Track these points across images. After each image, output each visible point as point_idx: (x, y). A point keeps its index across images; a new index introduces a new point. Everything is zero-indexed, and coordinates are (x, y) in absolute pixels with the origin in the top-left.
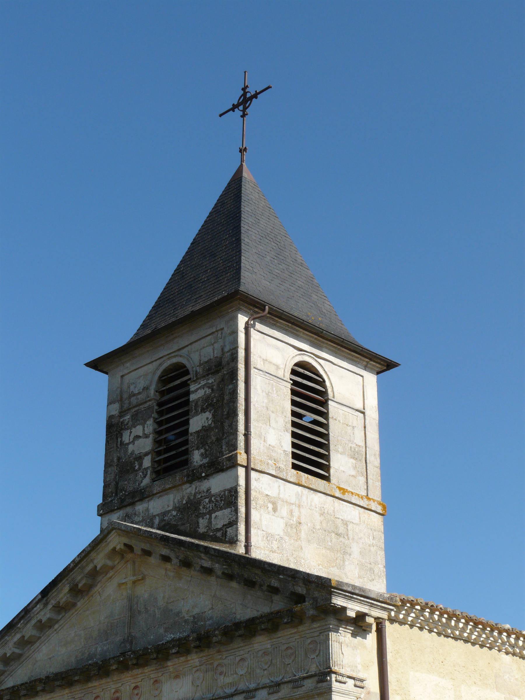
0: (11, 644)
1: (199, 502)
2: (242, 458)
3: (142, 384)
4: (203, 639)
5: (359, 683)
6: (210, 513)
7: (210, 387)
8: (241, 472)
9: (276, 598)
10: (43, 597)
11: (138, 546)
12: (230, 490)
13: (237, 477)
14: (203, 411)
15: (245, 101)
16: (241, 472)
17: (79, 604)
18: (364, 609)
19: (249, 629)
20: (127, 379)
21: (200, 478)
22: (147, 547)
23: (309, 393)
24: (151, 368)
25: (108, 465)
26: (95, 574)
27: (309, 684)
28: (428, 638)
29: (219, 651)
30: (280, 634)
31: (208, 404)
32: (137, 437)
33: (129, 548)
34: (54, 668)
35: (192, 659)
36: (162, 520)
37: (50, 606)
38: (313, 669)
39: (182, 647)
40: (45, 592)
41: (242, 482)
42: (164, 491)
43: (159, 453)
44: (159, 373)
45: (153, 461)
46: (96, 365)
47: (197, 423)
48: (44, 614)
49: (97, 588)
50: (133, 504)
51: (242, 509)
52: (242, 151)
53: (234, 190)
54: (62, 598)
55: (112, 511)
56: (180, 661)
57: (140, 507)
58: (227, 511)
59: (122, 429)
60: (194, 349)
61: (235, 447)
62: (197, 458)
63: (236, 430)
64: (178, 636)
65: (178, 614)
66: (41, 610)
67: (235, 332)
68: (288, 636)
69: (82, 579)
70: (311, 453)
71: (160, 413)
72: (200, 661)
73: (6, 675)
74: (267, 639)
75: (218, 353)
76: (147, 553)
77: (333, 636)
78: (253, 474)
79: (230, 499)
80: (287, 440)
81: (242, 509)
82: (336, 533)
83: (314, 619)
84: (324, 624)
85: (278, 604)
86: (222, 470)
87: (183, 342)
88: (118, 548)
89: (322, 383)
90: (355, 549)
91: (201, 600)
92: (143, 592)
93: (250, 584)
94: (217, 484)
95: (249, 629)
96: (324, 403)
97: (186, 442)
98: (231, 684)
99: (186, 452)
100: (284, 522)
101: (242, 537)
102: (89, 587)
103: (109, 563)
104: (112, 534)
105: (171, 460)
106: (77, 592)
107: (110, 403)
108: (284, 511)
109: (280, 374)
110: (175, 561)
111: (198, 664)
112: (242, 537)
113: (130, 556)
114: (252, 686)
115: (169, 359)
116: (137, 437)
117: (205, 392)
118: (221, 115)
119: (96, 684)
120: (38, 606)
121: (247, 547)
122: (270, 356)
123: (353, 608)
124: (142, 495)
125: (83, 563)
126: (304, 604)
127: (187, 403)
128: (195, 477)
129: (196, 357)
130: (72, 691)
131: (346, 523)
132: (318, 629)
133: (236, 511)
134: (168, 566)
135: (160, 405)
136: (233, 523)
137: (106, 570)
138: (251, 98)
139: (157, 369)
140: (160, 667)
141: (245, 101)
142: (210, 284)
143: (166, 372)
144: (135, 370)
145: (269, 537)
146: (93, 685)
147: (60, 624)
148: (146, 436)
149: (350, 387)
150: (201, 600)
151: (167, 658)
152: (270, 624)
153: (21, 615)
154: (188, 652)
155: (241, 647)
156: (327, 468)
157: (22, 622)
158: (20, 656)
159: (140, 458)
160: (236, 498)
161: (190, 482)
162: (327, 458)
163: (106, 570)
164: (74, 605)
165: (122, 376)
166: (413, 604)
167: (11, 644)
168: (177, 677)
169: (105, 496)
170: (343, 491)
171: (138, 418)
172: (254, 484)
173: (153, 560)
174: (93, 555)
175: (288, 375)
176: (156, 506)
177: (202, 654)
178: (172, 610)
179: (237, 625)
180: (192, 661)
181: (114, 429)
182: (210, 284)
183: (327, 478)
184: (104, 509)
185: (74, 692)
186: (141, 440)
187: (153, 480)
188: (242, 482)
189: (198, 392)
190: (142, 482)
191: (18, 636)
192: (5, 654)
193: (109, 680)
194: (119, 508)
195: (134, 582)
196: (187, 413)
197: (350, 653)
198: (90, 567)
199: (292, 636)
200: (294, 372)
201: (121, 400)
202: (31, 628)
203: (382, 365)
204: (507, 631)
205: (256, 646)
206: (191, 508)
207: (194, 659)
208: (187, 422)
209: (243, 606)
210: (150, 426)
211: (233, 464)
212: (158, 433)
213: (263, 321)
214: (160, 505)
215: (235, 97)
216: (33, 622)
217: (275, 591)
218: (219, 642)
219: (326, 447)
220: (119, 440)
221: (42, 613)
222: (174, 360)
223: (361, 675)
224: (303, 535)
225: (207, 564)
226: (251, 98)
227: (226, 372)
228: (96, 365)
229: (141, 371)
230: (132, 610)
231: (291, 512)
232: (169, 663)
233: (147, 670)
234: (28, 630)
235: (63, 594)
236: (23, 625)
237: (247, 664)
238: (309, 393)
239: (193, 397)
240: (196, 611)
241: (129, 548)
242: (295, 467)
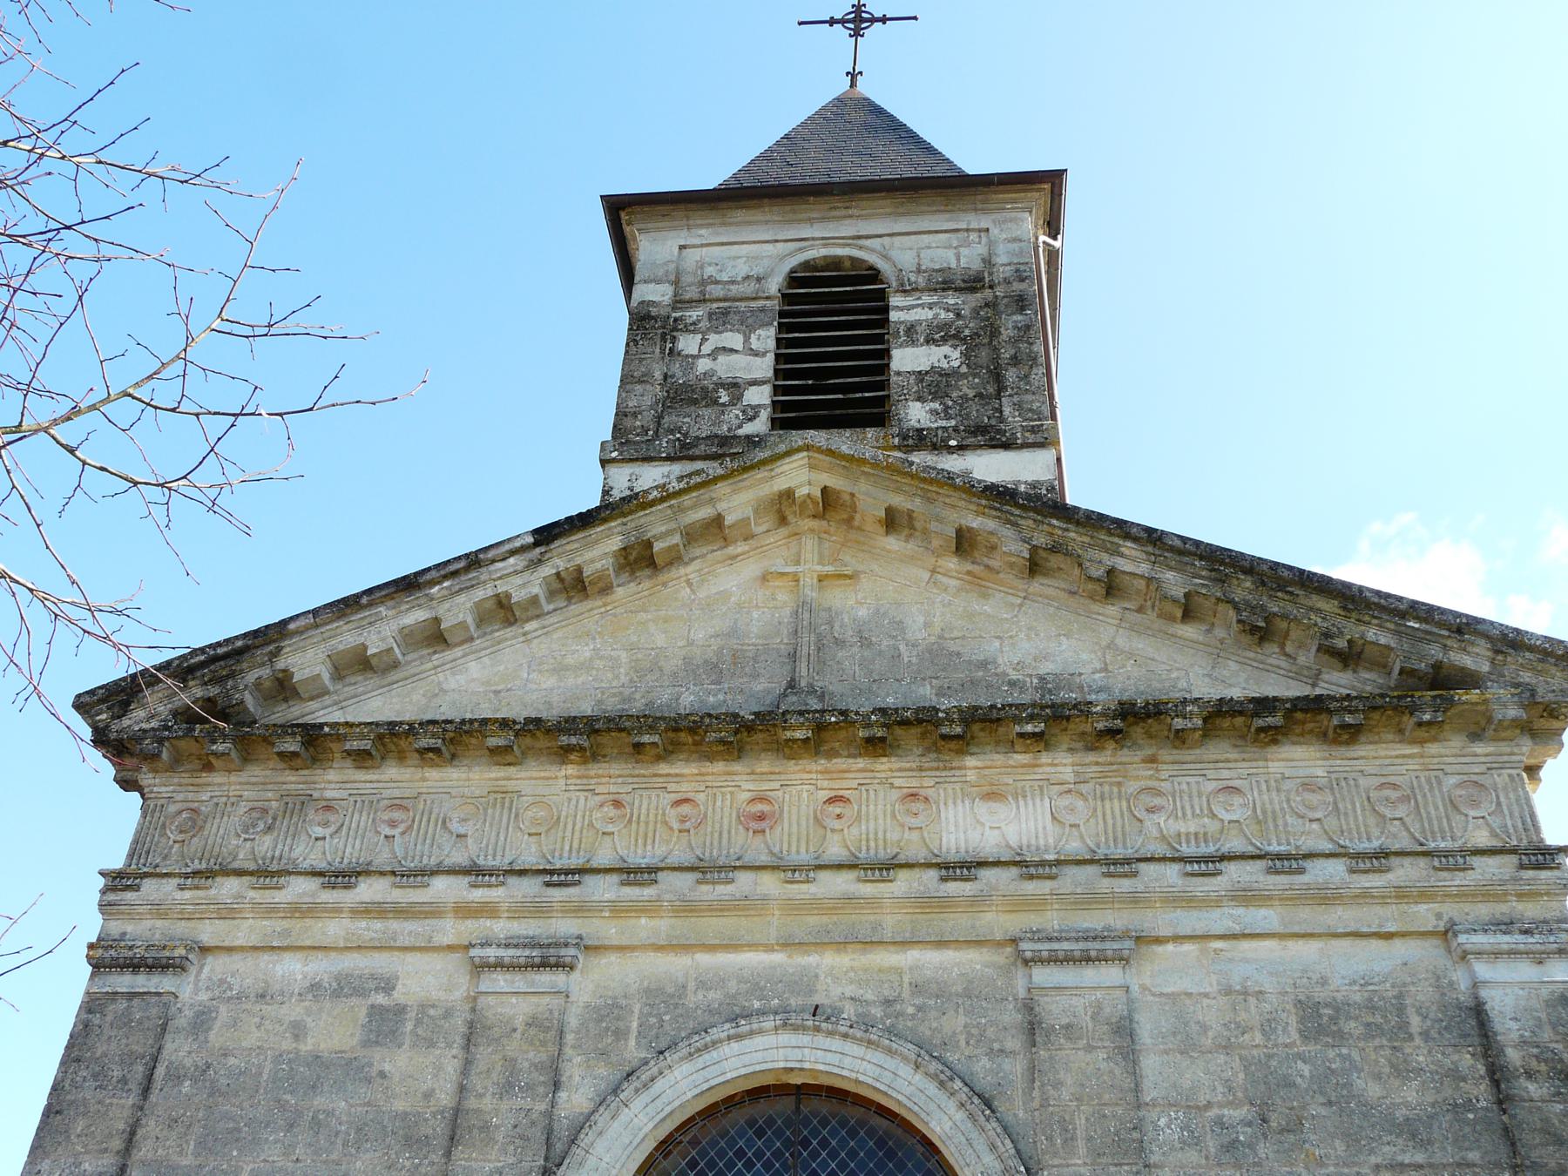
10: (536, 544)
17: (620, 592)
20: (693, 256)
29: (1152, 760)
30: (1362, 750)
35: (1052, 765)
37: (547, 570)
40: (546, 535)
48: (524, 584)
49: (690, 571)
54: (593, 561)
56: (1011, 762)
59: (675, 329)
65: (984, 665)
66: (516, 572)
69: (669, 533)
72: (1077, 773)
73: (328, 702)
74: (1318, 755)
75: (976, 265)
84: (1508, 750)
88: (802, 492)
92: (852, 605)
102: (675, 558)
104: (795, 457)
111: (1070, 777)
115: (825, 246)
117: (937, 315)
118: (800, 23)
119: (686, 771)
120: (512, 560)
125: (687, 500)
127: (885, 322)
130: (592, 773)
132: (1483, 759)
139: (790, 254)
140: (935, 764)
144: (723, 244)
146: (672, 771)
147: (546, 623)
153: (452, 568)
155: (1228, 761)
157: (446, 584)
159: (736, 388)
164: (606, 589)
165: (682, 247)
168: (992, 796)
177: (1091, 757)
178: (958, 654)
180: (1048, 769)
185: (599, 776)
190: (740, 427)
192: (365, 648)
193: (737, 767)
198: (705, 513)
199: (1400, 761)
202: (469, 605)
205: (1275, 767)
210: (766, 338)
216: (480, 594)
220: (669, 345)
221: (518, 580)
232: (970, 761)
234: (457, 609)
236: (445, 592)
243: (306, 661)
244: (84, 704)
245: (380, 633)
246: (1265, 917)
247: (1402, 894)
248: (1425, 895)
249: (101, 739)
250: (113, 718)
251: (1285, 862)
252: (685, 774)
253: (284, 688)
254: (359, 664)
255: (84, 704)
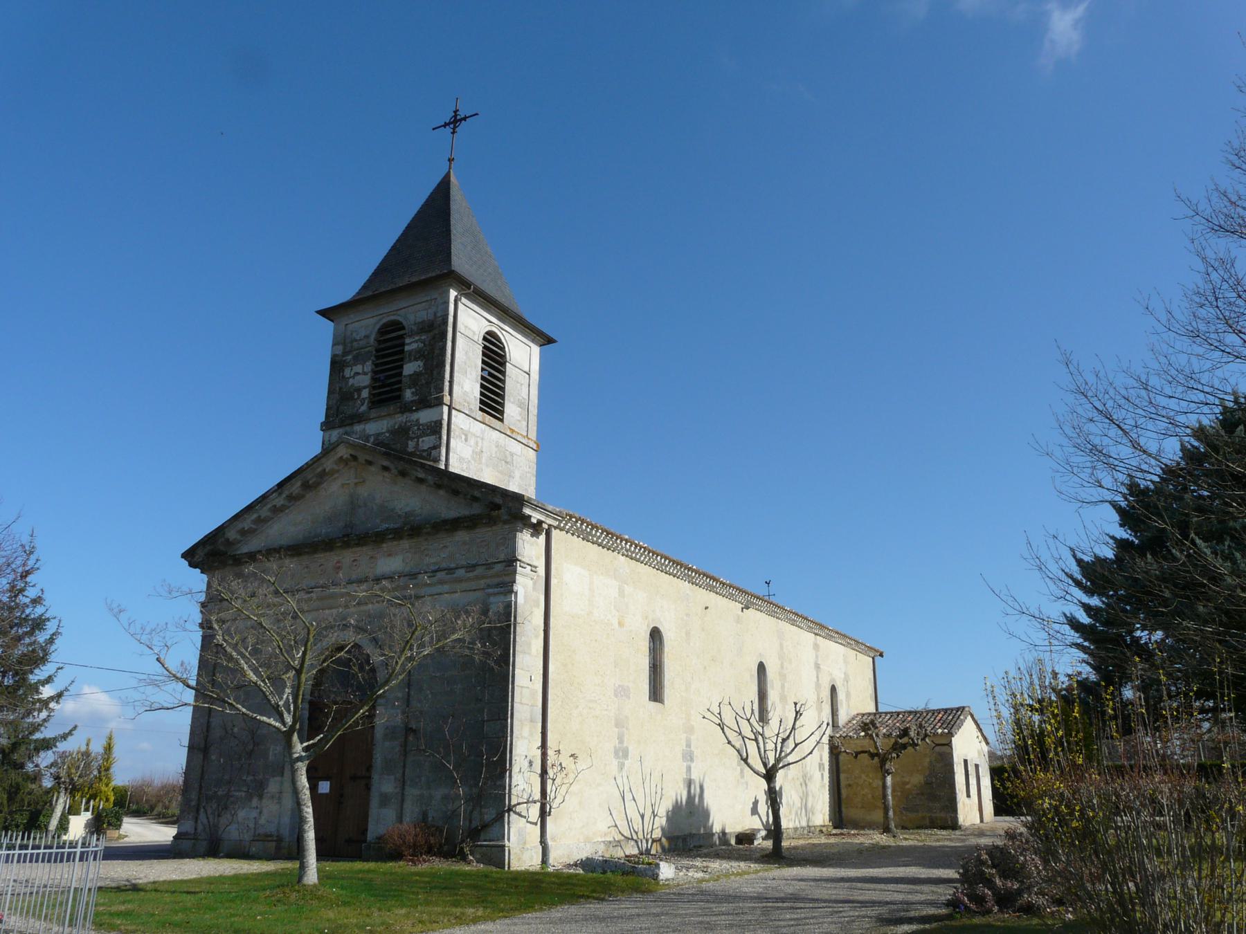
0: (249, 521)
1: (409, 429)
2: (447, 399)
3: (363, 333)
4: (414, 529)
5: (534, 568)
6: (418, 438)
7: (423, 342)
8: (445, 409)
9: (475, 505)
11: (362, 457)
12: (436, 422)
13: (442, 413)
14: (416, 359)
15: (455, 122)
16: (445, 409)
18: (542, 518)
19: (454, 525)
20: (350, 327)
21: (411, 411)
22: (370, 458)
23: (494, 356)
24: (372, 321)
25: (330, 392)
26: (323, 475)
27: (499, 567)
28: (577, 541)
31: (418, 355)
32: (358, 374)
33: (354, 458)
34: (284, 541)
36: (376, 439)
38: (502, 557)
39: (397, 534)
40: (281, 485)
41: (445, 417)
42: (380, 417)
43: (374, 388)
44: (378, 327)
45: (370, 393)
46: (325, 313)
47: (410, 368)
48: (279, 501)
49: (324, 485)
50: (352, 424)
51: (444, 437)
52: (450, 160)
53: (442, 192)
55: (334, 428)
57: (358, 428)
58: (433, 438)
60: (411, 311)
61: (442, 390)
62: (408, 395)
63: (443, 377)
64: (392, 526)
65: (392, 510)
67: (447, 303)
68: (483, 533)
70: (492, 401)
71: (377, 357)
75: (431, 317)
76: (370, 463)
77: (519, 535)
78: (454, 412)
79: (435, 428)
80: (478, 389)
81: (444, 437)
82: (506, 460)
83: (505, 522)
85: (476, 509)
86: (430, 407)
87: (403, 304)
89: (503, 349)
90: (517, 474)
91: (410, 500)
92: (363, 491)
93: (456, 493)
94: (425, 416)
95: (454, 525)
96: (503, 364)
97: (400, 382)
98: (435, 563)
99: (400, 389)
100: (479, 450)
101: (443, 458)
103: (336, 467)
105: (387, 392)
106: (307, 486)
107: (334, 345)
108: (472, 441)
109: (476, 338)
110: (394, 471)
112: (443, 458)
113: (353, 464)
114: (453, 565)
116: (358, 374)
121: (447, 465)
122: (471, 323)
123: (535, 516)
124: (360, 418)
126: (497, 511)
127: (402, 351)
128: (406, 408)
129: (412, 318)
131: (512, 455)
133: (440, 438)
134: (386, 474)
135: (377, 351)
136: (438, 447)
137: (333, 472)
138: (461, 120)
141: (455, 122)
142: (422, 259)
143: (386, 325)
145: (461, 459)
148: (365, 374)
149: (522, 354)
150: (410, 500)
151: (383, 541)
152: (470, 523)
154: (401, 538)
156: (502, 413)
158: (255, 530)
159: (359, 390)
160: (441, 428)
161: (402, 413)
162: (502, 405)
163: (333, 472)
164: (303, 496)
166: (571, 517)
167: (249, 521)
168: (390, 555)
169: (327, 416)
170: (513, 431)
171: (358, 359)
172: (453, 419)
173: (373, 469)
174: (323, 460)
175: (481, 341)
176: (372, 428)
179: (445, 522)
181: (337, 366)
182: (422, 259)
183: (501, 420)
184: (327, 426)
186: (361, 376)
187: (370, 408)
188: (445, 417)
189: (411, 345)
191: (255, 516)
194: (340, 427)
195: (356, 484)
196: (402, 360)
197: (529, 547)
198: (319, 470)
200: (485, 339)
201: (344, 344)
203: (545, 340)
204: (627, 541)
206: (402, 432)
207: (406, 543)
208: (401, 367)
209: (448, 509)
210: (369, 366)
211: (440, 403)
212: (375, 372)
213: (468, 296)
214: (377, 427)
215: (448, 117)
217: (475, 499)
218: (428, 533)
219: (503, 397)
222: (392, 318)
223: (534, 563)
224: (484, 460)
225: (421, 475)
226: (461, 120)
227: (437, 334)
228: (325, 313)
229: (364, 323)
230: (353, 504)
231: (477, 443)
233: (365, 549)
234: (264, 512)
235: (296, 487)
237: (455, 548)
238: (494, 356)
239: (407, 348)
240: (408, 509)
241: (354, 458)
242: (481, 409)
243: (232, 535)
244: (184, 556)
245: (247, 524)
246: (446, 587)
247: (477, 578)
248: (483, 577)
249: (191, 565)
250: (192, 556)
251: (450, 571)
252: (321, 557)
253: (228, 543)
254: (243, 533)
255: (184, 556)
